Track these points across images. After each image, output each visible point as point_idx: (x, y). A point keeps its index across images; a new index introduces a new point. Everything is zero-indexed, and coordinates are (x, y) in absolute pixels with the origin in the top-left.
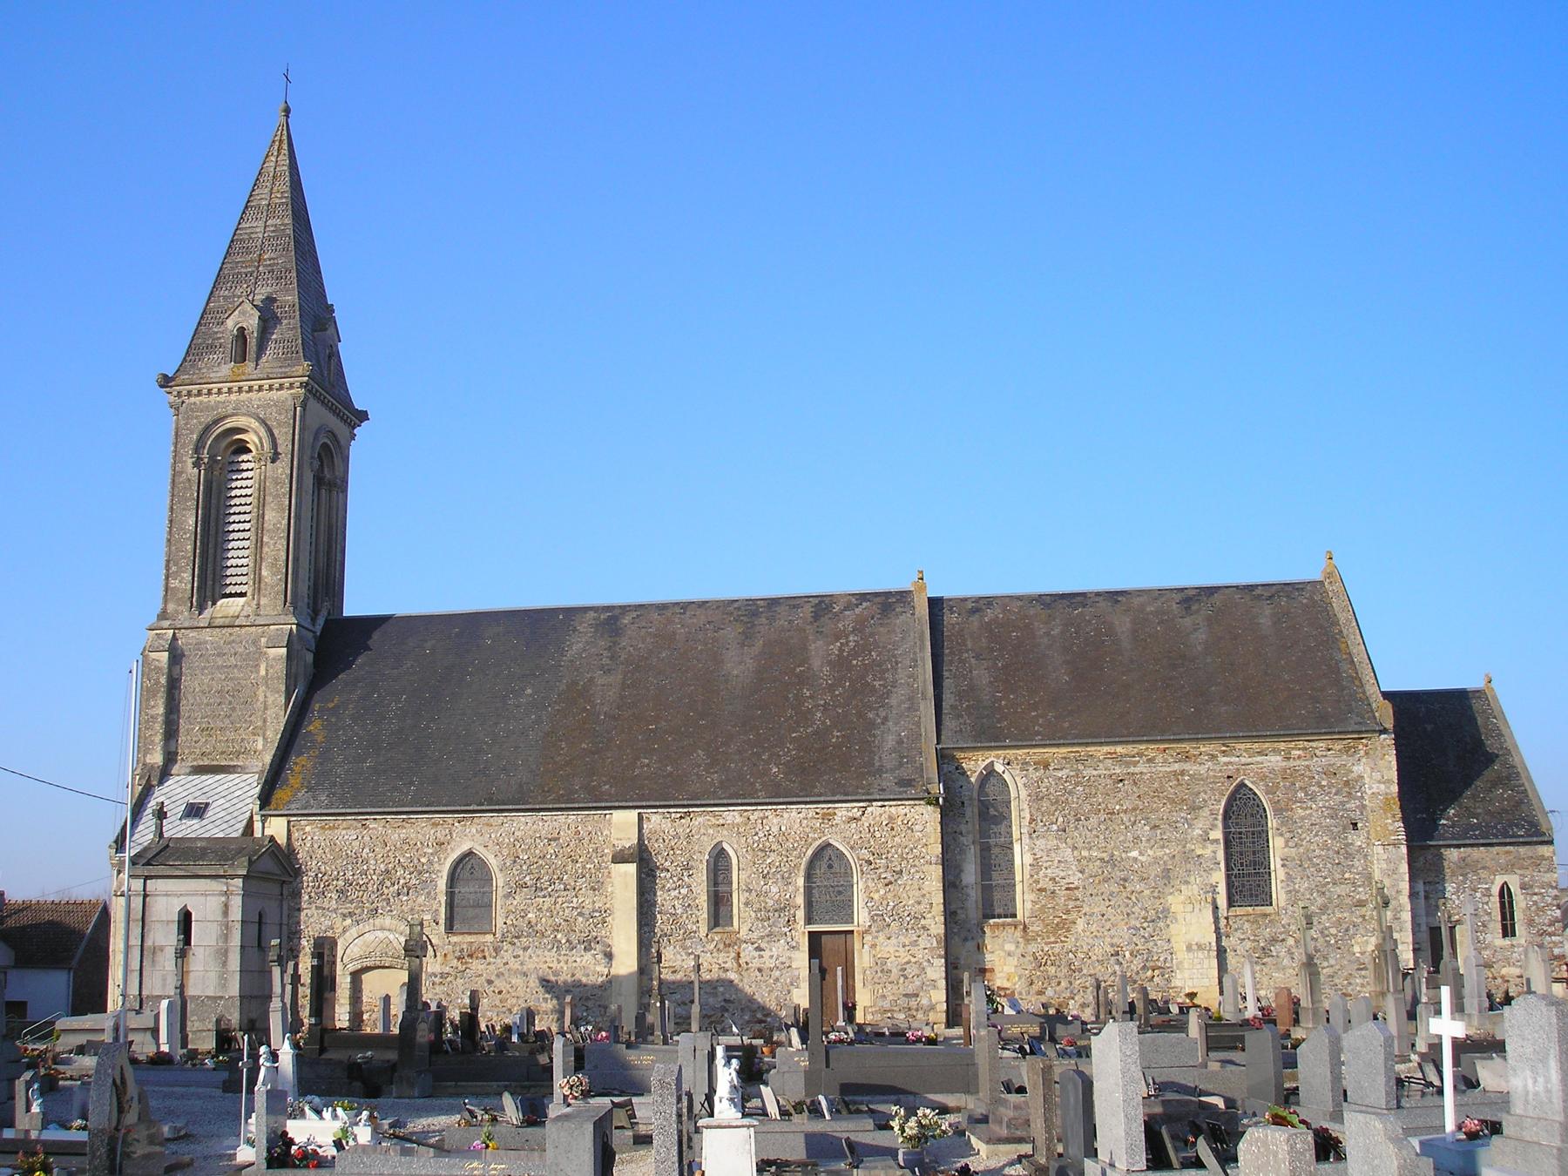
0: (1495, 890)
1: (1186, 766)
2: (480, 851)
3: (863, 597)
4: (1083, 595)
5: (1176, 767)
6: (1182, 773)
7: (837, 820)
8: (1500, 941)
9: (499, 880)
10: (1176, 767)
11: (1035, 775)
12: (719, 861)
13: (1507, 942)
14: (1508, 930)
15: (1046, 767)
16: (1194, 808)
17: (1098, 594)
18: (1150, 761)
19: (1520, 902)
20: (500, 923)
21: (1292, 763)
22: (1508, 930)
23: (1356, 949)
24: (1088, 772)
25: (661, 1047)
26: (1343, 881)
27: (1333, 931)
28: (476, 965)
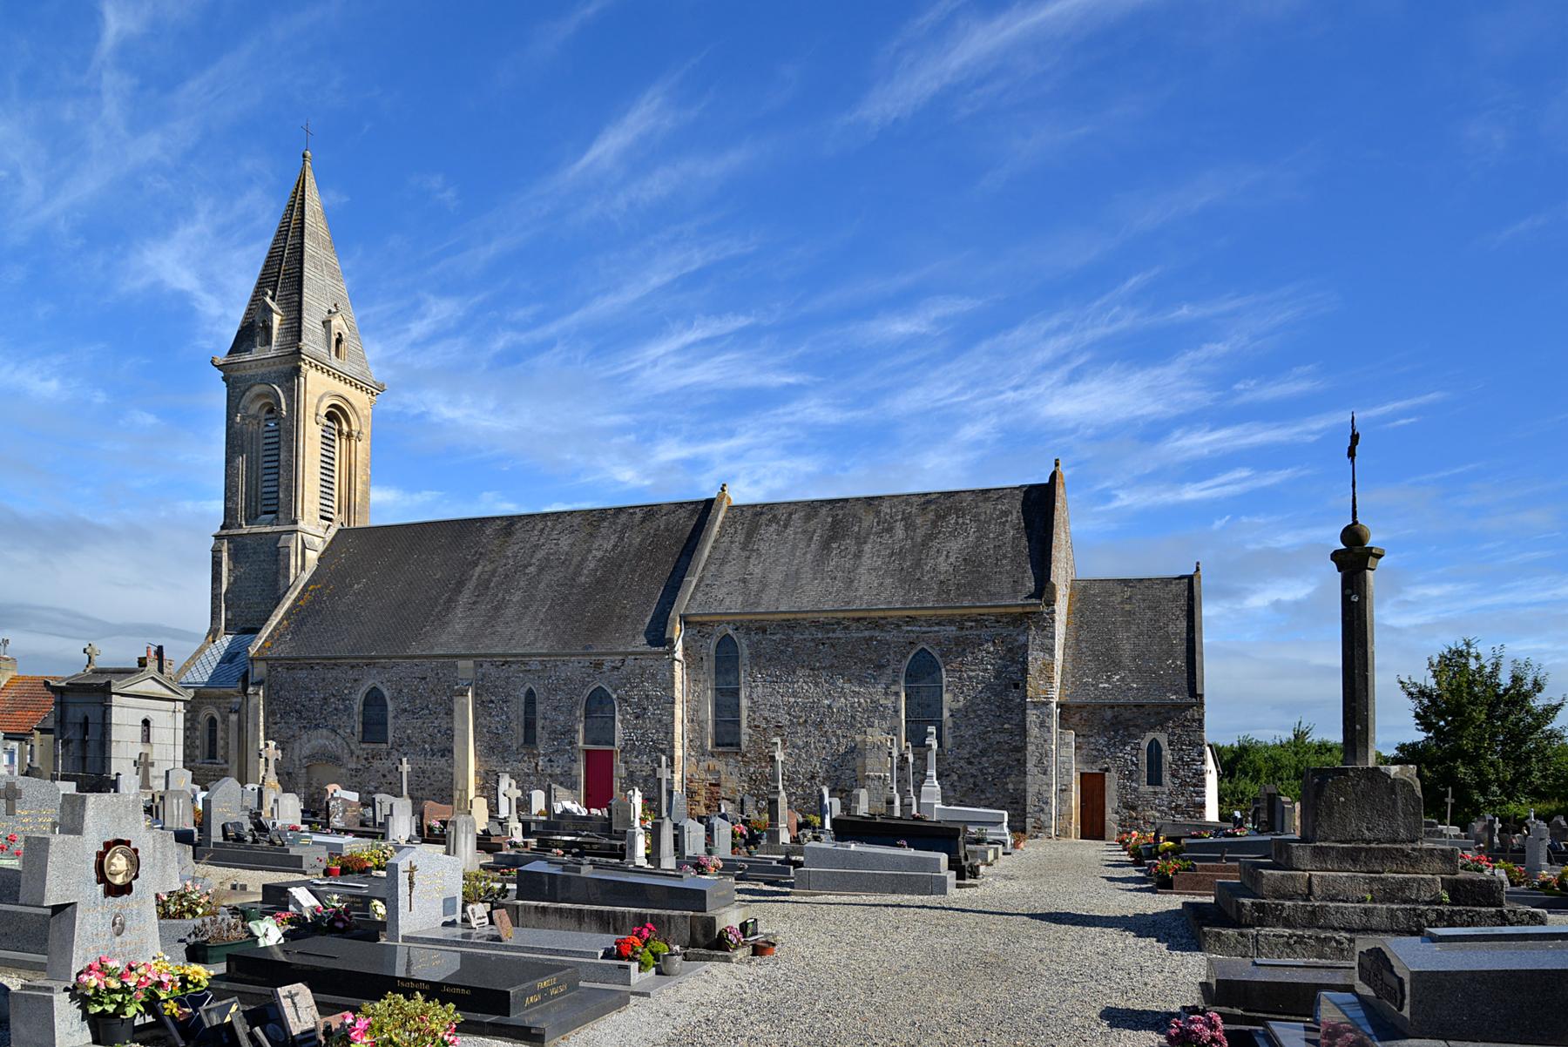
0: (1145, 744)
1: (872, 633)
2: (379, 686)
3: (681, 505)
4: (846, 500)
5: (867, 634)
6: (871, 638)
7: (605, 668)
8: (1145, 788)
9: (390, 707)
10: (867, 634)
11: (755, 638)
12: (530, 698)
13: (1151, 789)
14: (1155, 779)
15: (764, 631)
16: (880, 667)
17: (858, 499)
18: (846, 628)
19: (1167, 755)
20: (390, 735)
21: (964, 633)
22: (1155, 779)
23: (1010, 786)
24: (797, 637)
25: (954, 894)
26: (1003, 731)
27: (991, 770)
28: (376, 764)
